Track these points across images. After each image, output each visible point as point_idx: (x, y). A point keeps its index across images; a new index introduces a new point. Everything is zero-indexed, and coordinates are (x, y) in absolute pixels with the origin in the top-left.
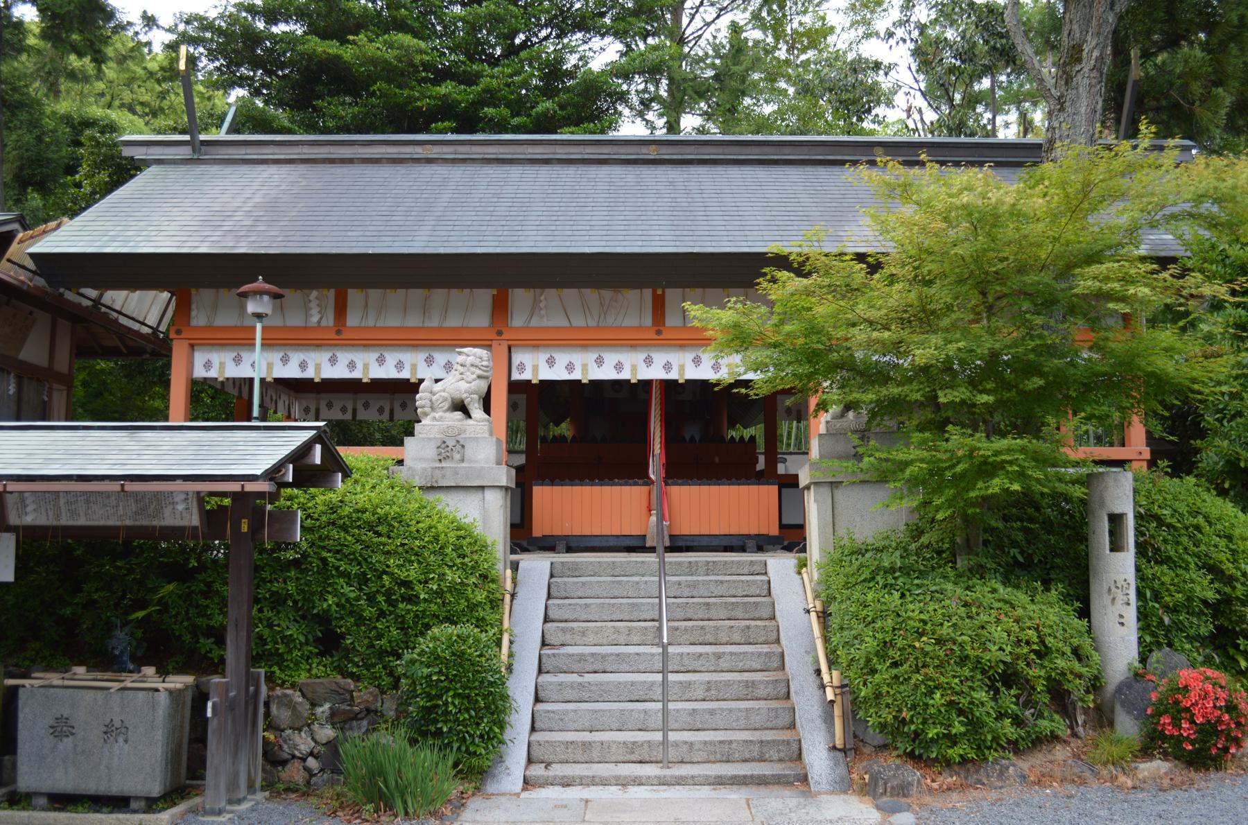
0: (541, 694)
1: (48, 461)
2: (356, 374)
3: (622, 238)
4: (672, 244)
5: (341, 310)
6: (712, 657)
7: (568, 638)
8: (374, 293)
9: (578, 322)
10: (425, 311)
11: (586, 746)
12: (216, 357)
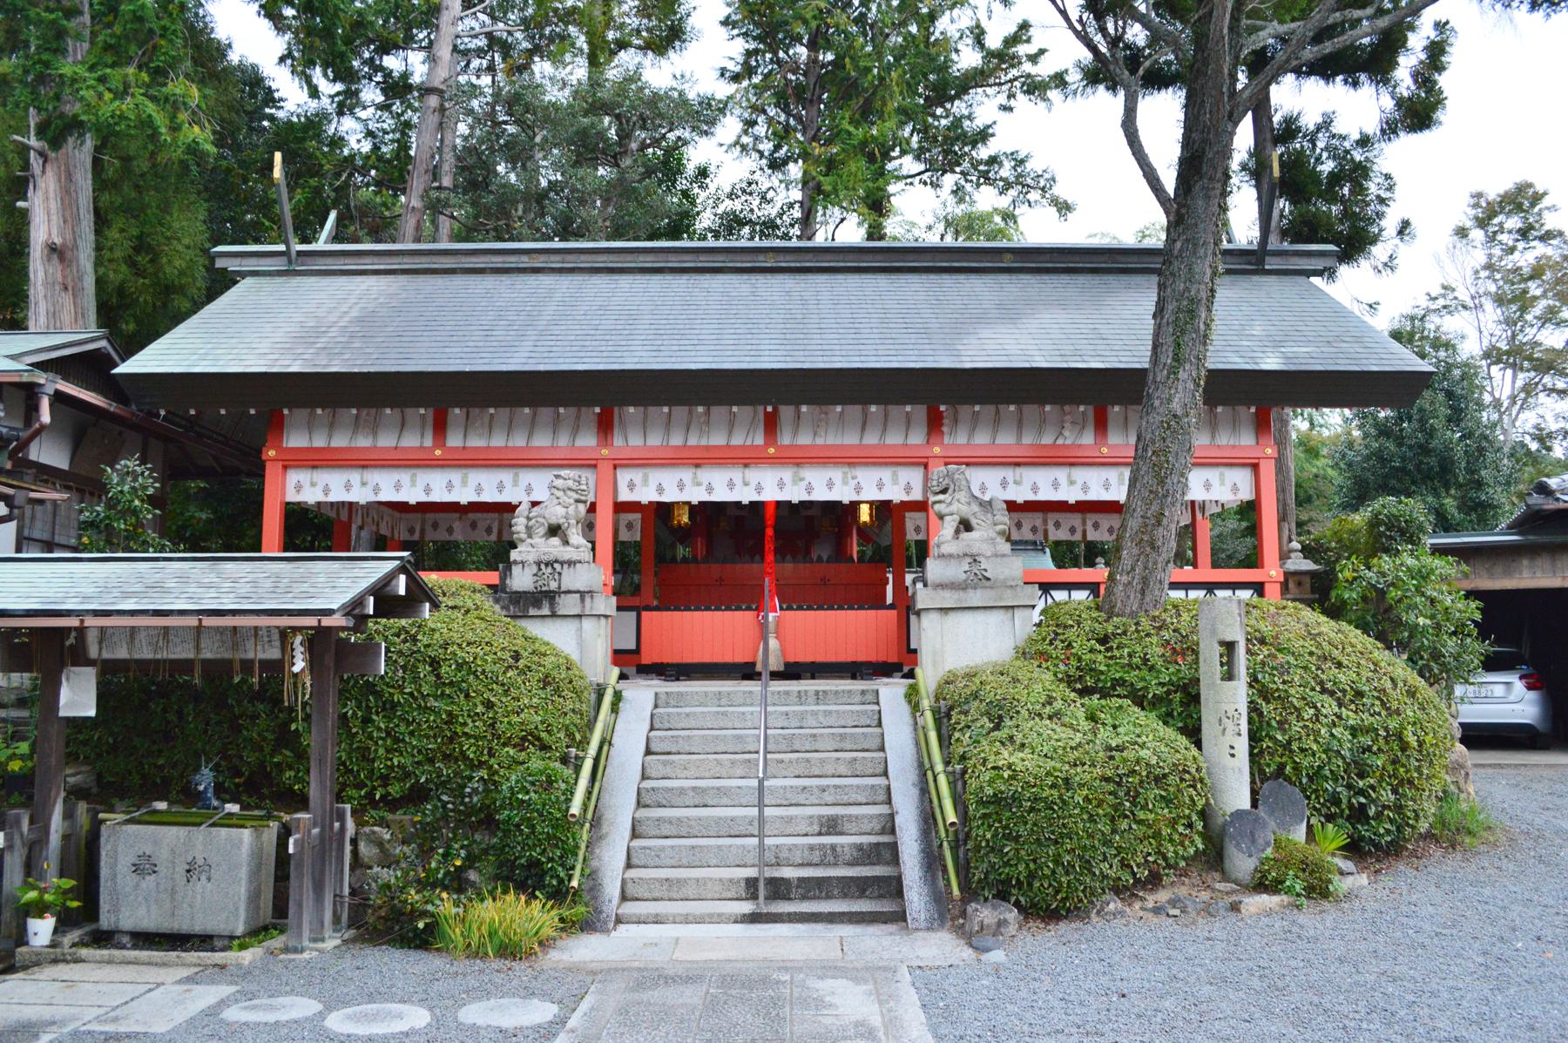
0: (639, 829)
1: (127, 595)
3: (730, 353)
4: (783, 359)
6: (816, 790)
7: (668, 771)
9: (738, 440)
11: (681, 882)
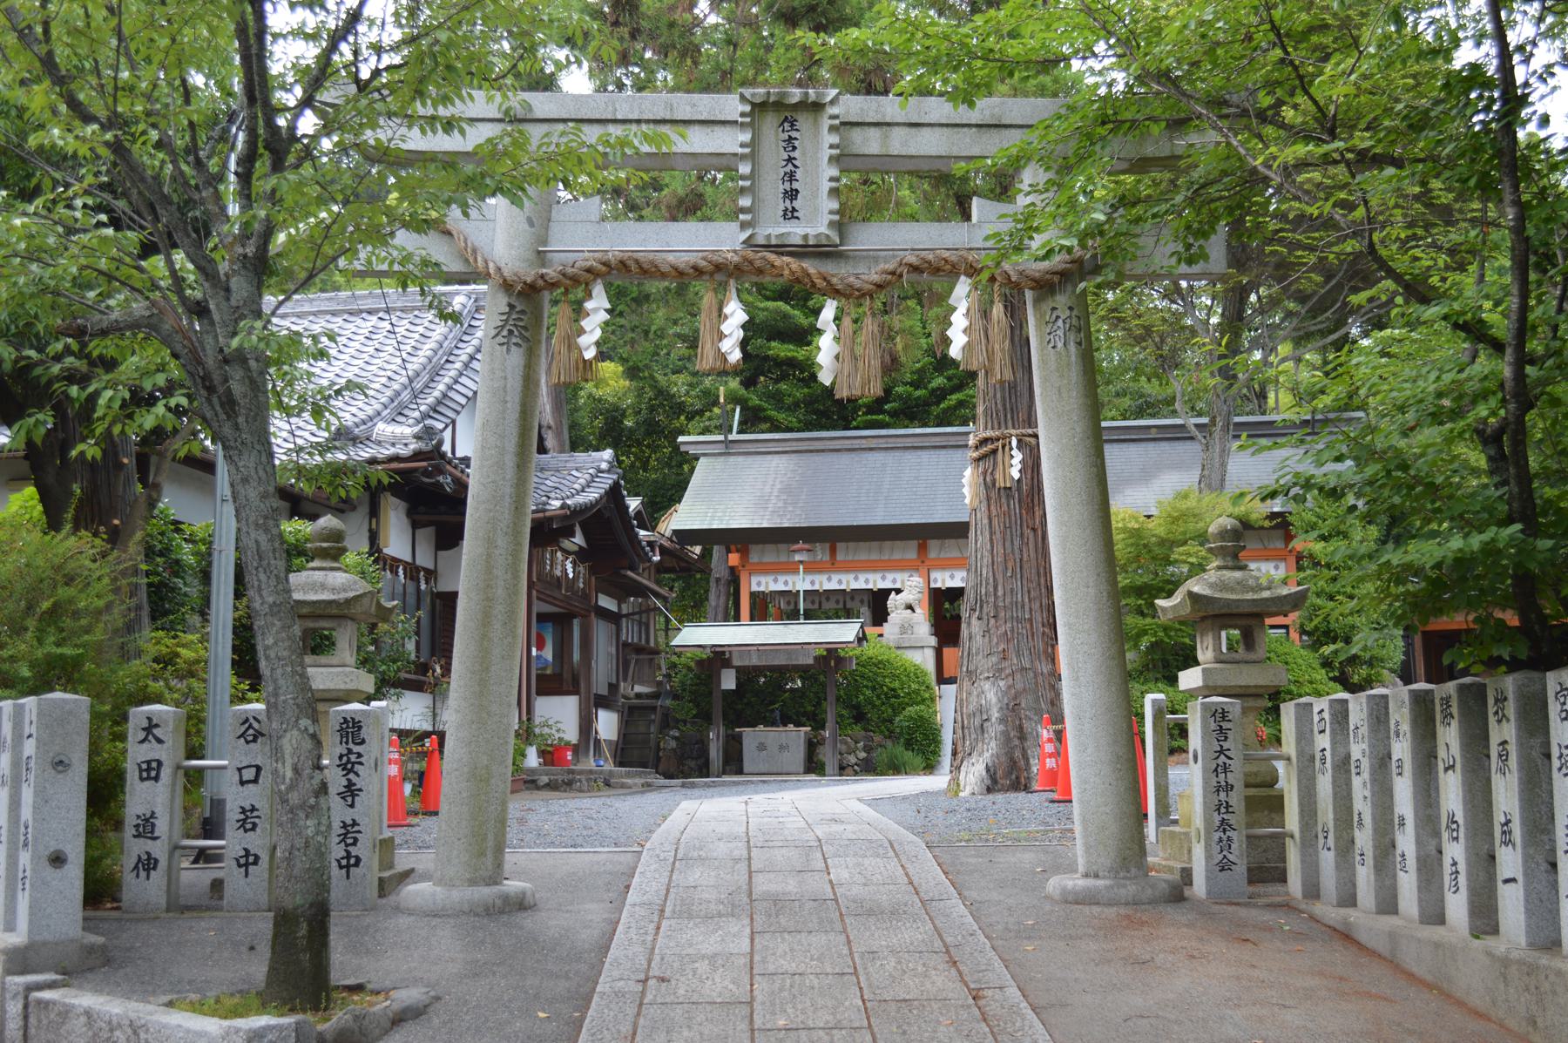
2: (843, 587)
5: (833, 551)
8: (851, 544)
10: (881, 550)
12: (763, 579)
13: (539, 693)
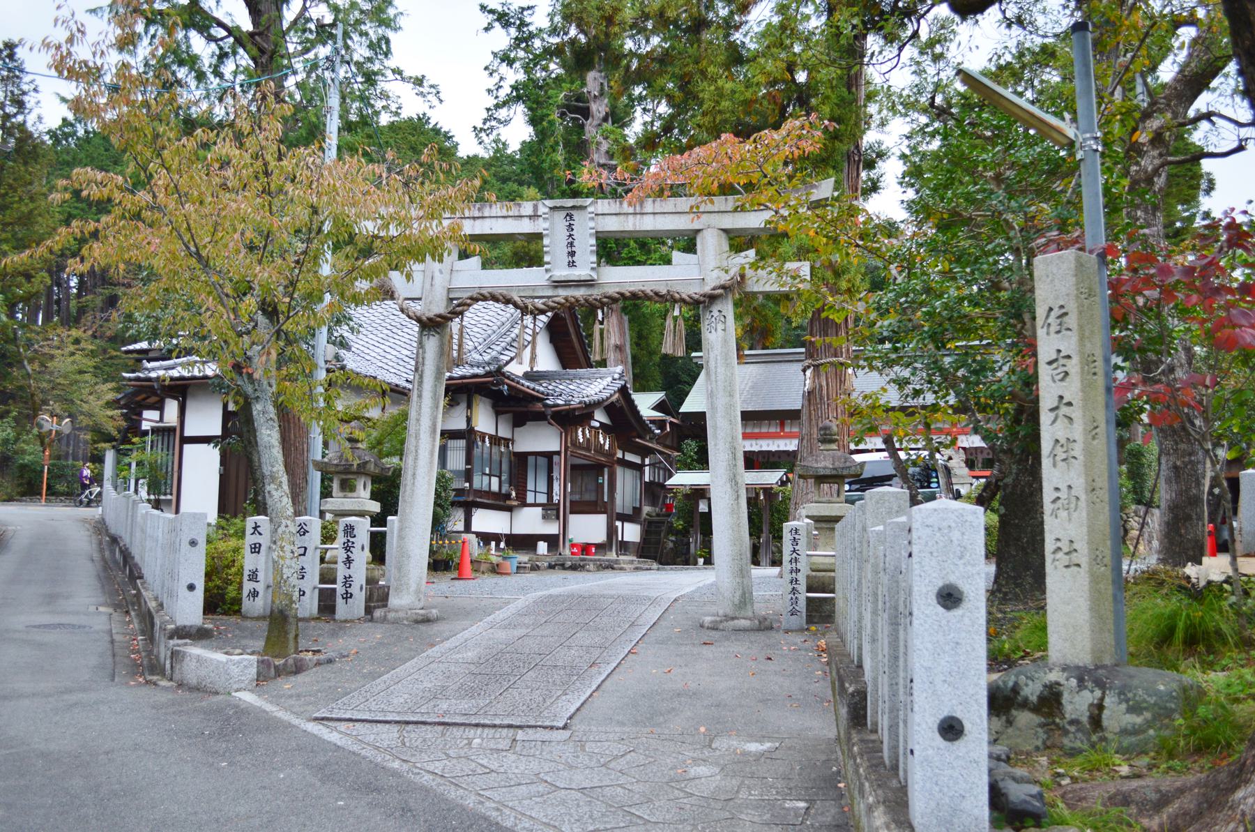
13: (572, 512)
